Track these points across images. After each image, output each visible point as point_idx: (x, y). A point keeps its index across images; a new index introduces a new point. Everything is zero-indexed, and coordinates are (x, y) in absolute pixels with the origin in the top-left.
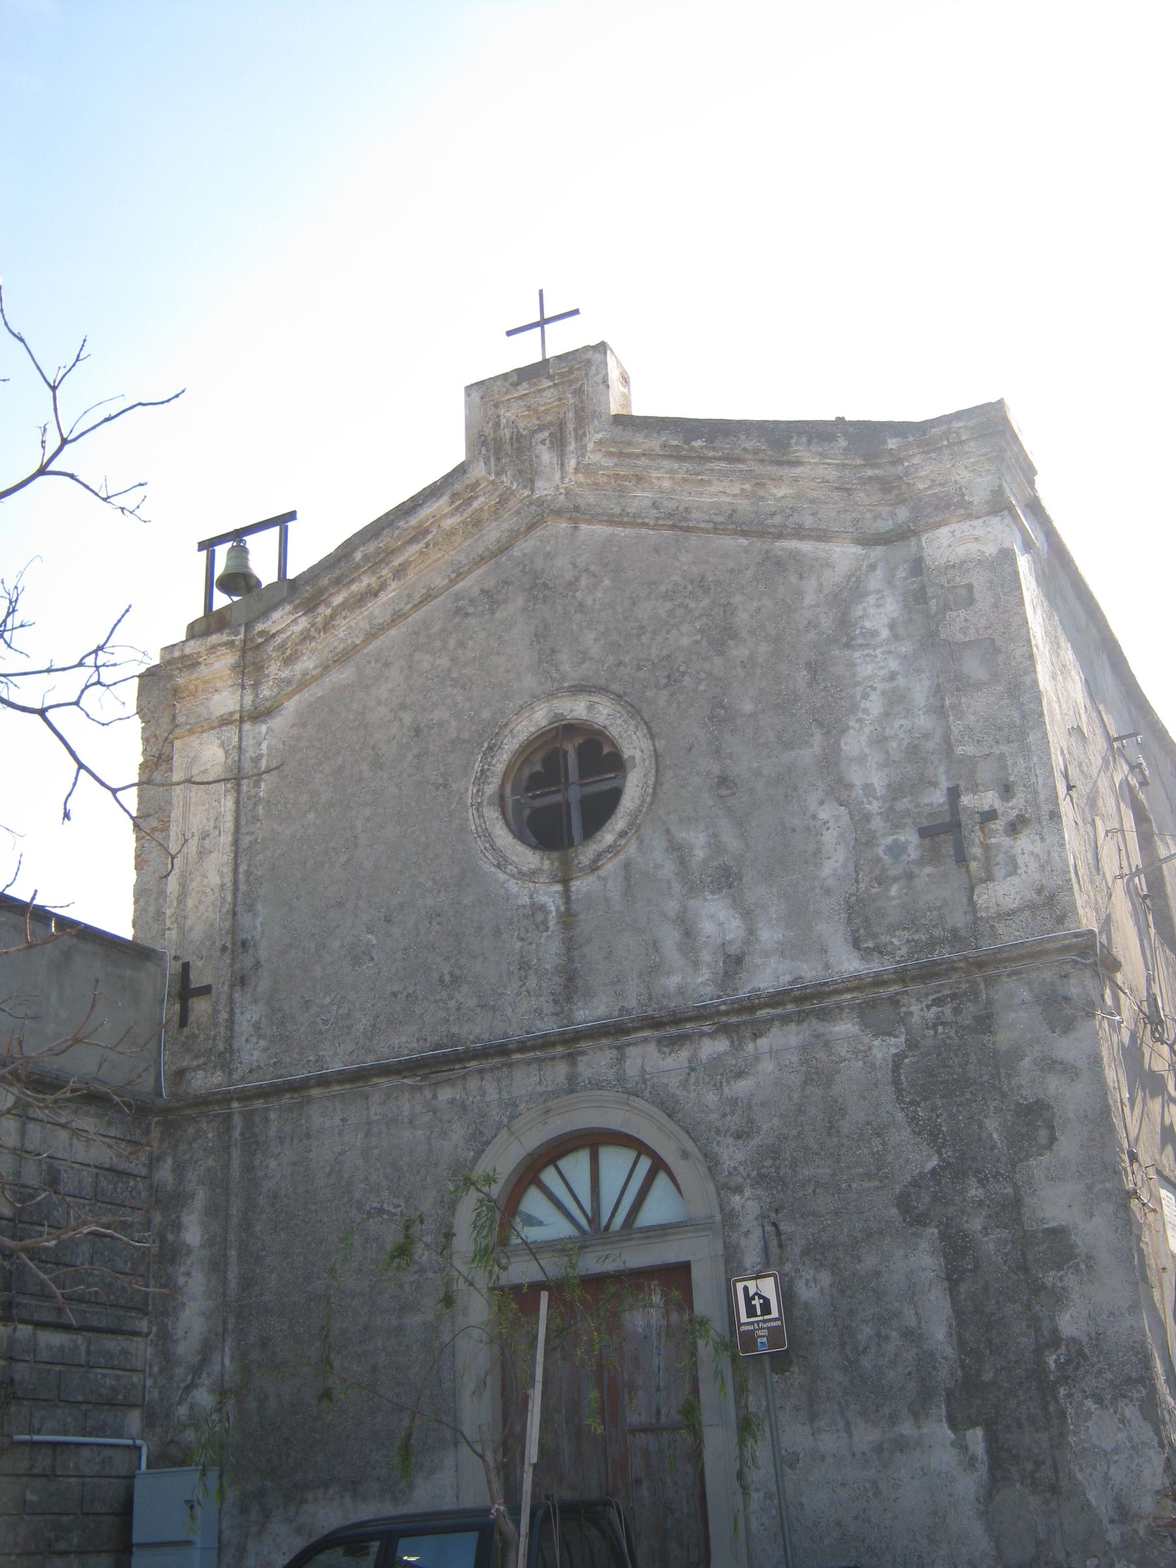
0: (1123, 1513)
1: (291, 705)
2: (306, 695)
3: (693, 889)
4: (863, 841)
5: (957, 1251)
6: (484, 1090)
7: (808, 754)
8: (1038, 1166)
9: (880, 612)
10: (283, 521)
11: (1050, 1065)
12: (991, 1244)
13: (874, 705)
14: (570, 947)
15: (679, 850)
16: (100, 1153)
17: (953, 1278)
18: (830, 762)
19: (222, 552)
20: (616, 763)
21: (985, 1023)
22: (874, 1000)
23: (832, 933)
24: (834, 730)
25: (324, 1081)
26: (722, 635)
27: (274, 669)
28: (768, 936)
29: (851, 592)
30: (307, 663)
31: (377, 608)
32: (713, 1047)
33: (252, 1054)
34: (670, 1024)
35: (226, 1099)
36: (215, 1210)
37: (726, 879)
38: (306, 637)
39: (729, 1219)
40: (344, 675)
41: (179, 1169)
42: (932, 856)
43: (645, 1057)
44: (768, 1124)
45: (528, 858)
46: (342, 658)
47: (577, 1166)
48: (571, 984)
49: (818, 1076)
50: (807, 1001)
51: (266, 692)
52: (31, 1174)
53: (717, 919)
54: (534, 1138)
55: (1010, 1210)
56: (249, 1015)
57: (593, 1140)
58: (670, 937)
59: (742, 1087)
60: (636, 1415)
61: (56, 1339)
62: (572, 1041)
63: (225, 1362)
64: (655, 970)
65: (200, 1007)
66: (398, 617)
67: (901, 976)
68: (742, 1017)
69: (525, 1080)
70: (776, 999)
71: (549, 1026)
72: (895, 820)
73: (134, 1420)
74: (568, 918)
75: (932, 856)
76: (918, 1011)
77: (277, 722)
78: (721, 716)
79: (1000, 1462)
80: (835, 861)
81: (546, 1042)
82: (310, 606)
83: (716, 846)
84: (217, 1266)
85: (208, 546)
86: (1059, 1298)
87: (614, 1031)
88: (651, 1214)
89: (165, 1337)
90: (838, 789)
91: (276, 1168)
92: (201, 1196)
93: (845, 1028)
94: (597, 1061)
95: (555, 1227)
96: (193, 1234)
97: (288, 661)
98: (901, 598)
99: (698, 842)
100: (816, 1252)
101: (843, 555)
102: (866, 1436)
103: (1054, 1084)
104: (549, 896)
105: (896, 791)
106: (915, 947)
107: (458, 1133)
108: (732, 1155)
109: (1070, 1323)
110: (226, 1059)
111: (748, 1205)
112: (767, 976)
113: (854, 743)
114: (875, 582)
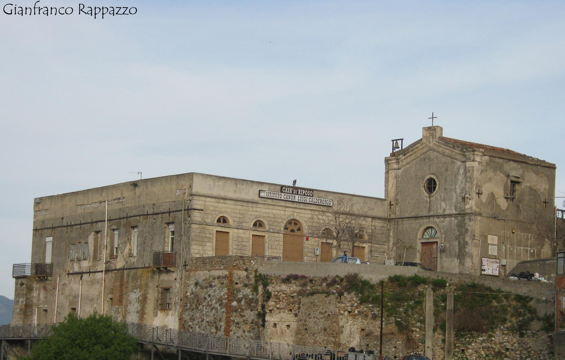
0: (468, 268)
1: (402, 169)
2: (405, 167)
3: (441, 201)
4: (457, 198)
5: (459, 242)
6: (421, 221)
7: (453, 187)
8: (466, 235)
9: (462, 171)
10: (402, 140)
11: (469, 225)
12: (462, 242)
13: (460, 182)
14: (430, 205)
15: (440, 196)
16: (381, 225)
17: (459, 245)
18: (455, 188)
19: (395, 142)
20: (434, 181)
21: (464, 220)
22: (456, 216)
23: (453, 208)
24: (456, 185)
25: (405, 218)
26: (447, 170)
27: (400, 163)
28: (448, 207)
29: (459, 168)
30: (404, 163)
31: (413, 157)
32: (442, 219)
33: (398, 213)
34: (438, 216)
35: (395, 219)
36: (394, 231)
37: (445, 200)
38: (404, 159)
39: (442, 237)
40: (408, 166)
41: (390, 226)
42: (462, 201)
43: (436, 220)
44: (446, 228)
45: (427, 194)
46: (408, 163)
47: (430, 230)
48: (430, 210)
49: (450, 223)
50: (450, 215)
51: (400, 166)
52: (373, 228)
53: (443, 204)
54: (425, 227)
55: (464, 239)
56: (397, 209)
57: (431, 228)
58: (439, 206)
59: (444, 224)
60: (433, 256)
61: (376, 245)
62: (429, 217)
63: (395, 248)
64: (437, 210)
65: (392, 207)
66: (414, 159)
67: (458, 214)
68: (444, 216)
69: (425, 220)
70: (447, 215)
71: (427, 215)
72: (460, 196)
73: (385, 254)
74: (430, 202)
75: (462, 201)
76: (459, 218)
77: (401, 171)
78: (446, 180)
79: (460, 262)
80: (454, 200)
81: (426, 216)
82: (405, 155)
83: (444, 196)
84: (394, 238)
85: (393, 141)
86: (466, 248)
87: (433, 216)
88: (436, 236)
89: (388, 245)
90: (455, 192)
91: (400, 227)
92: (392, 230)
93: (453, 219)
94: (431, 219)
95: (428, 237)
96: (391, 234)
97: (402, 162)
98: (539, 193)
99: (442, 195)
100: (448, 242)
101: (459, 163)
102: (450, 259)
103: (469, 227)
104: (428, 199)
105: (460, 193)
106: (460, 211)
107: (418, 225)
108: (442, 231)
109: (467, 250)
110: (395, 214)
111: (443, 236)
112: (447, 212)
113: (457, 187)
114: (462, 167)
